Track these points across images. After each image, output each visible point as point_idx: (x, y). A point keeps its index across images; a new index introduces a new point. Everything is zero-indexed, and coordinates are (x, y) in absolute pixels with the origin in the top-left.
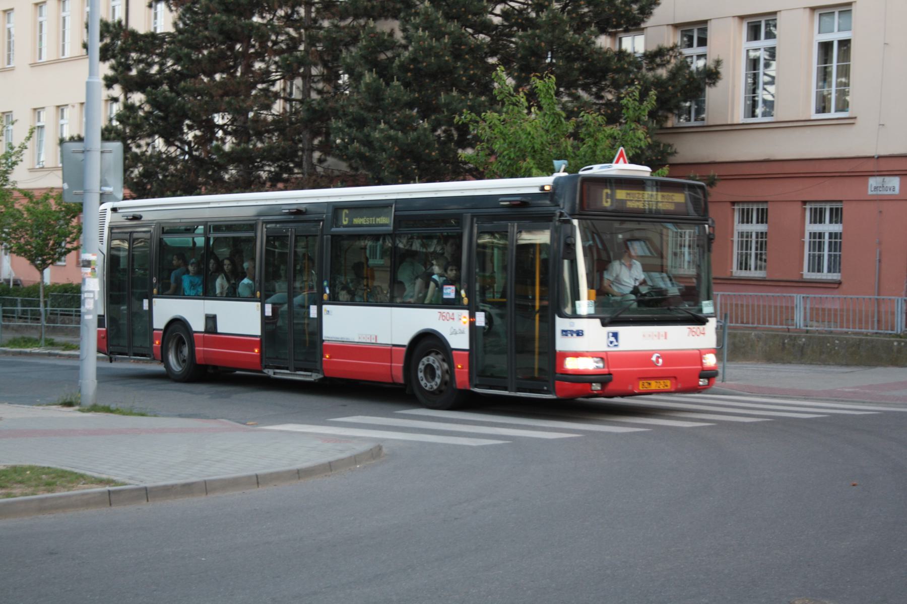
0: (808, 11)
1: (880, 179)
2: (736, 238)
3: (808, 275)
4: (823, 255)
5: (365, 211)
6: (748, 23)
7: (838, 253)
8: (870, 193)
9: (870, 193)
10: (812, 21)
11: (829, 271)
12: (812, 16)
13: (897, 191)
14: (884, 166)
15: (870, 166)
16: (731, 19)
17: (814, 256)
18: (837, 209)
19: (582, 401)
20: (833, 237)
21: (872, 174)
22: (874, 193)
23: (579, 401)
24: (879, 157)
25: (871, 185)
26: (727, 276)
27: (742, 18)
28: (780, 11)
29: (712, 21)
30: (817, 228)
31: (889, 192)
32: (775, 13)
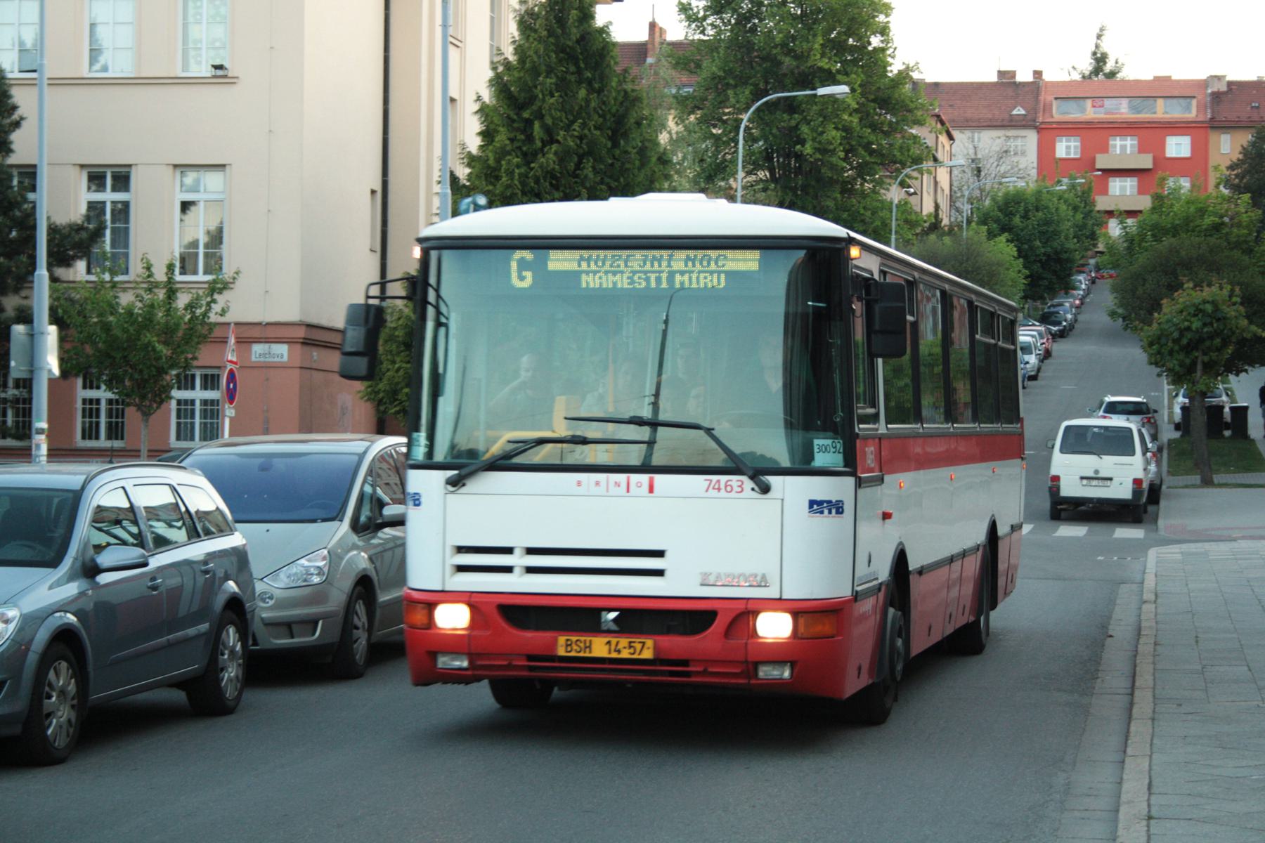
0: (171, 167)
1: (267, 346)
2: (79, 405)
3: (81, 443)
4: (201, 419)
5: (279, 365)
6: (89, 172)
7: (120, 420)
8: (253, 359)
9: (253, 359)
10: (174, 177)
11: (109, 437)
12: (174, 172)
13: (285, 358)
14: (271, 333)
15: (256, 333)
16: (72, 168)
17: (205, 424)
18: (213, 376)
19: (388, 600)
20: (94, 403)
21: (258, 341)
22: (258, 360)
23: (385, 601)
24: (268, 324)
25: (256, 352)
26: (73, 447)
27: (82, 166)
28: (136, 165)
29: (139, 167)
30: (92, 394)
31: (276, 360)
32: (130, 166)
